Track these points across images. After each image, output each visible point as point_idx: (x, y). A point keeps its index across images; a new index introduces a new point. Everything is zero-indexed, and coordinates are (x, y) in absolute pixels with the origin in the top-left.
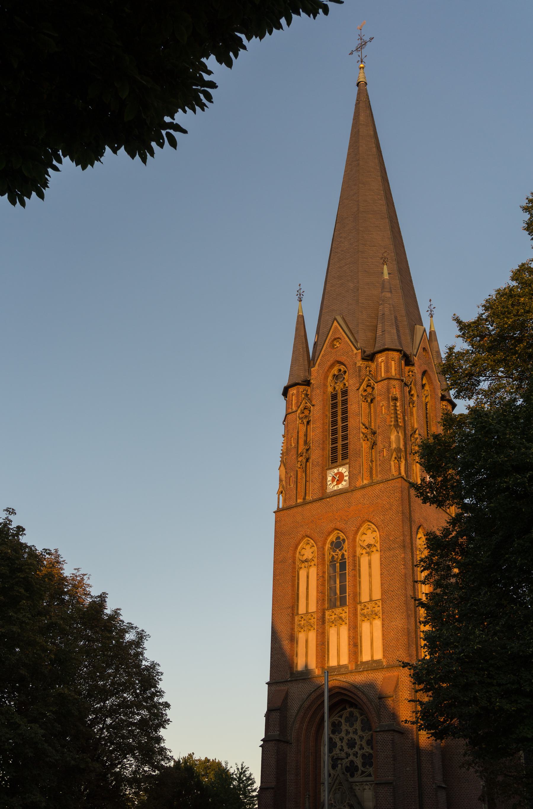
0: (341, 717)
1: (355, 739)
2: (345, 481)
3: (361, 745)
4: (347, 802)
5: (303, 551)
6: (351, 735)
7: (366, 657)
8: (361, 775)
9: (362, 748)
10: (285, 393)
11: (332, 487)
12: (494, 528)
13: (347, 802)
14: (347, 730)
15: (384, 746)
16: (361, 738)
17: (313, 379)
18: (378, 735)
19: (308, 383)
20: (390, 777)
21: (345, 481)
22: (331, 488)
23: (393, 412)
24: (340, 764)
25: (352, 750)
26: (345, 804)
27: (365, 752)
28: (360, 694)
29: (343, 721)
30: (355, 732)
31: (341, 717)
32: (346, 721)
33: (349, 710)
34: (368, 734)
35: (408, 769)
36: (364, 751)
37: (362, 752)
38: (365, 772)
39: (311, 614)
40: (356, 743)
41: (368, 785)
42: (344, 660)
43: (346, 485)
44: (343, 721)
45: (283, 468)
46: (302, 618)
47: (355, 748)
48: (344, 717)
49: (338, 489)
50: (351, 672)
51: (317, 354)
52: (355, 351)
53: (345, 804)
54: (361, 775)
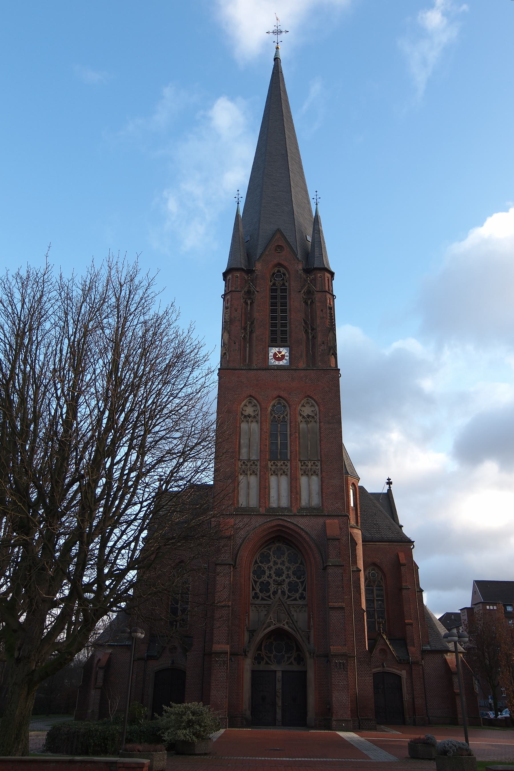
0: (270, 549)
1: (282, 569)
2: (286, 360)
4: (286, 621)
5: (245, 408)
9: (288, 576)
12: (18, 459)
13: (286, 621)
14: (275, 561)
15: (335, 578)
18: (330, 568)
19: (250, 271)
20: (340, 604)
21: (286, 360)
22: (273, 362)
24: (280, 589)
26: (285, 622)
27: (292, 580)
28: (303, 534)
30: (283, 563)
31: (270, 551)
34: (295, 566)
36: (291, 579)
37: (289, 581)
39: (245, 461)
40: (283, 573)
41: (294, 607)
43: (286, 363)
46: (244, 463)
47: (282, 576)
49: (279, 364)
50: (295, 515)
53: (285, 622)
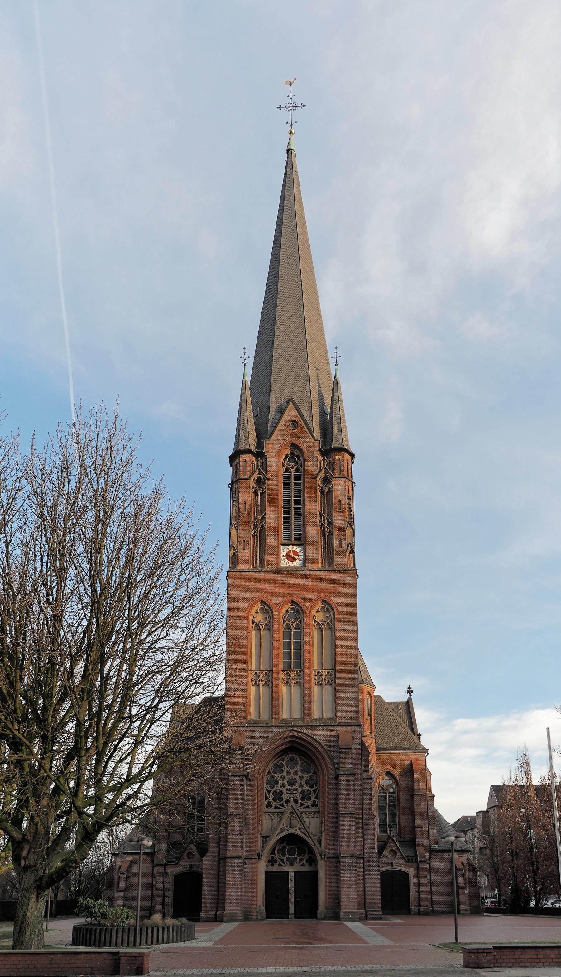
3: (301, 784)
6: (292, 775)
7: (316, 714)
8: (300, 806)
10: (232, 458)
11: (285, 563)
14: (288, 771)
16: (301, 778)
17: (267, 452)
23: (347, 509)
25: (292, 787)
26: (297, 828)
29: (284, 764)
31: (283, 761)
32: (287, 764)
33: (290, 755)
35: (356, 804)
36: (304, 788)
38: (304, 805)
42: (297, 715)
44: (284, 764)
45: (234, 531)
48: (285, 761)
51: (310, 425)
52: (313, 441)
54: (300, 806)
